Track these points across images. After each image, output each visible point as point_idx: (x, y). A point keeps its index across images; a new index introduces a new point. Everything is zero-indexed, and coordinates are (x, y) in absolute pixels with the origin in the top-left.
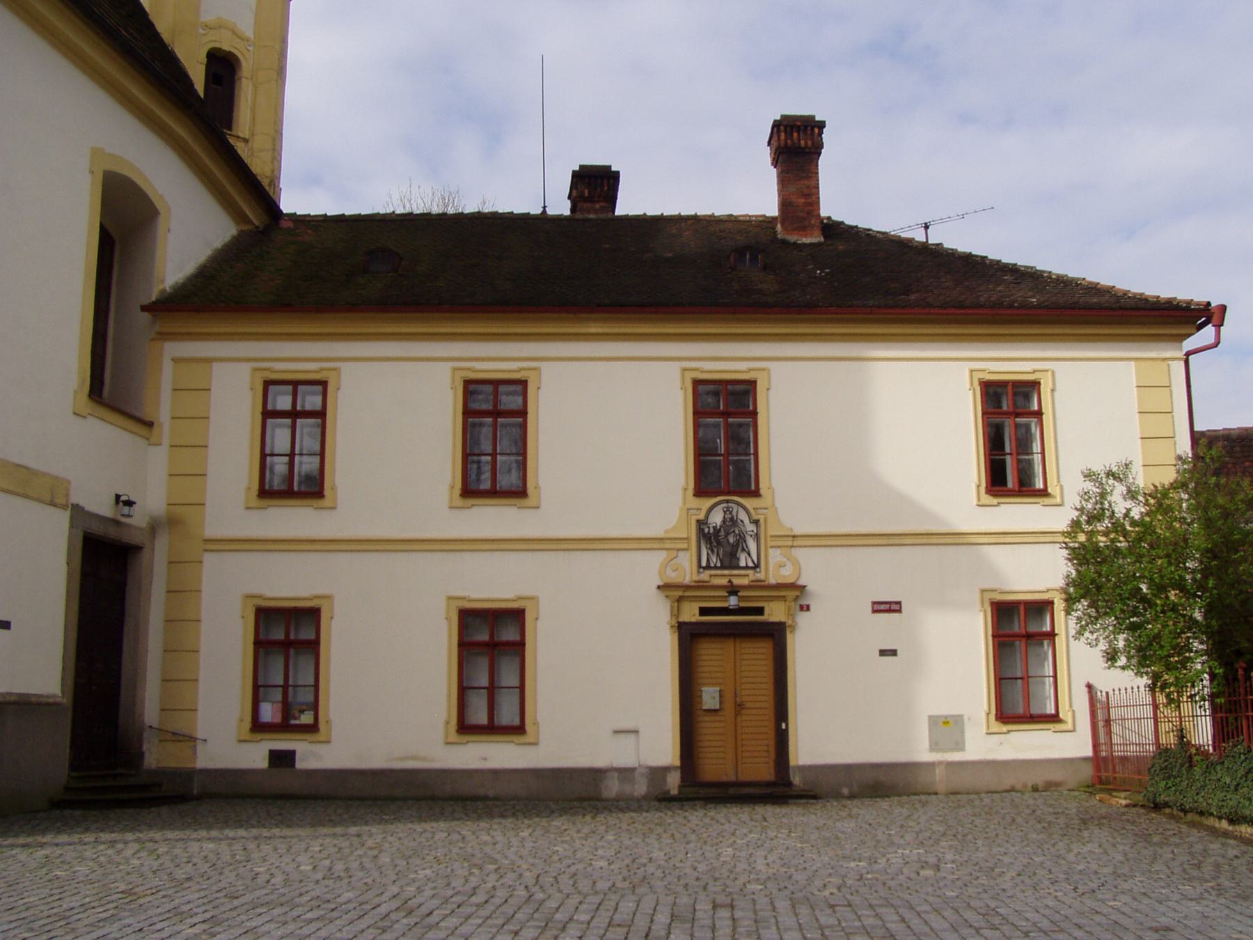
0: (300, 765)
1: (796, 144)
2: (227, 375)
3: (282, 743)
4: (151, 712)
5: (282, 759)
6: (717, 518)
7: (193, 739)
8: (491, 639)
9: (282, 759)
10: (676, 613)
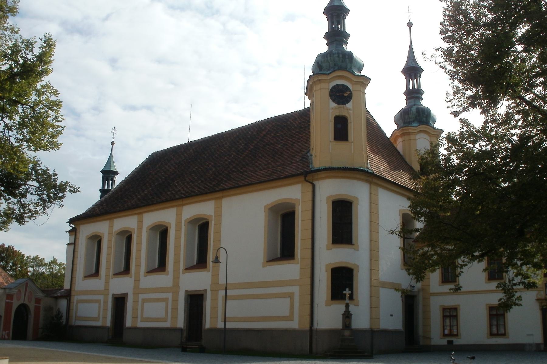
0: (455, 343)
3: (450, 339)
5: (450, 342)
9: (450, 342)
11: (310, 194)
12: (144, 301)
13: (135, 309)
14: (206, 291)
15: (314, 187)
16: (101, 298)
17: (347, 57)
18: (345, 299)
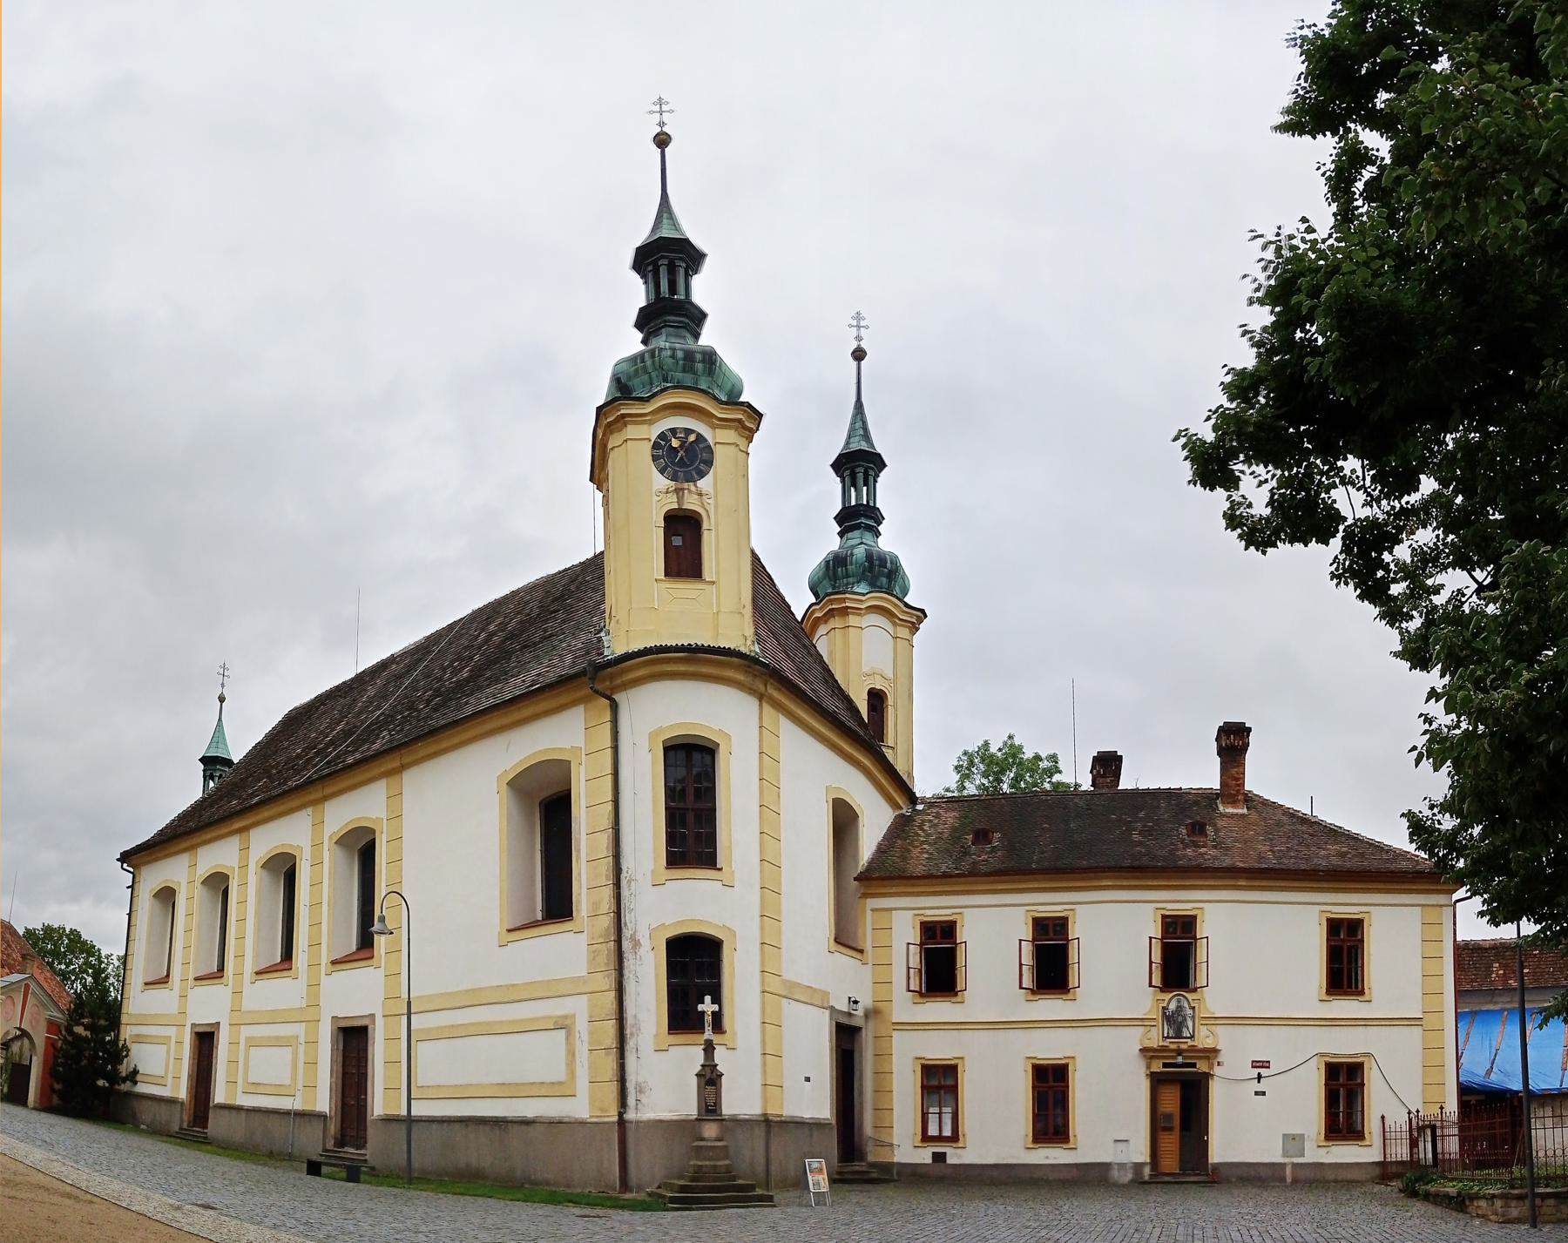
0: (949, 1161)
1: (1233, 742)
2: (899, 923)
4: (868, 1129)
5: (939, 1158)
6: (1173, 1006)
7: (891, 1145)
8: (1051, 1084)
9: (939, 1158)
10: (1148, 1067)
11: (607, 729)
12: (253, 1043)
13: (233, 1062)
14: (372, 1016)
15: (614, 707)
16: (171, 1032)
17: (699, 357)
18: (701, 1030)
